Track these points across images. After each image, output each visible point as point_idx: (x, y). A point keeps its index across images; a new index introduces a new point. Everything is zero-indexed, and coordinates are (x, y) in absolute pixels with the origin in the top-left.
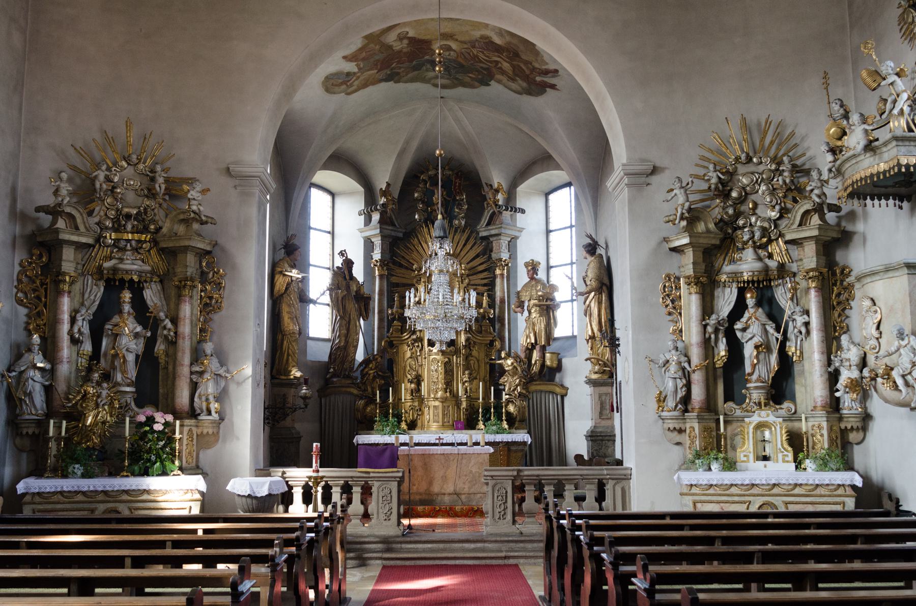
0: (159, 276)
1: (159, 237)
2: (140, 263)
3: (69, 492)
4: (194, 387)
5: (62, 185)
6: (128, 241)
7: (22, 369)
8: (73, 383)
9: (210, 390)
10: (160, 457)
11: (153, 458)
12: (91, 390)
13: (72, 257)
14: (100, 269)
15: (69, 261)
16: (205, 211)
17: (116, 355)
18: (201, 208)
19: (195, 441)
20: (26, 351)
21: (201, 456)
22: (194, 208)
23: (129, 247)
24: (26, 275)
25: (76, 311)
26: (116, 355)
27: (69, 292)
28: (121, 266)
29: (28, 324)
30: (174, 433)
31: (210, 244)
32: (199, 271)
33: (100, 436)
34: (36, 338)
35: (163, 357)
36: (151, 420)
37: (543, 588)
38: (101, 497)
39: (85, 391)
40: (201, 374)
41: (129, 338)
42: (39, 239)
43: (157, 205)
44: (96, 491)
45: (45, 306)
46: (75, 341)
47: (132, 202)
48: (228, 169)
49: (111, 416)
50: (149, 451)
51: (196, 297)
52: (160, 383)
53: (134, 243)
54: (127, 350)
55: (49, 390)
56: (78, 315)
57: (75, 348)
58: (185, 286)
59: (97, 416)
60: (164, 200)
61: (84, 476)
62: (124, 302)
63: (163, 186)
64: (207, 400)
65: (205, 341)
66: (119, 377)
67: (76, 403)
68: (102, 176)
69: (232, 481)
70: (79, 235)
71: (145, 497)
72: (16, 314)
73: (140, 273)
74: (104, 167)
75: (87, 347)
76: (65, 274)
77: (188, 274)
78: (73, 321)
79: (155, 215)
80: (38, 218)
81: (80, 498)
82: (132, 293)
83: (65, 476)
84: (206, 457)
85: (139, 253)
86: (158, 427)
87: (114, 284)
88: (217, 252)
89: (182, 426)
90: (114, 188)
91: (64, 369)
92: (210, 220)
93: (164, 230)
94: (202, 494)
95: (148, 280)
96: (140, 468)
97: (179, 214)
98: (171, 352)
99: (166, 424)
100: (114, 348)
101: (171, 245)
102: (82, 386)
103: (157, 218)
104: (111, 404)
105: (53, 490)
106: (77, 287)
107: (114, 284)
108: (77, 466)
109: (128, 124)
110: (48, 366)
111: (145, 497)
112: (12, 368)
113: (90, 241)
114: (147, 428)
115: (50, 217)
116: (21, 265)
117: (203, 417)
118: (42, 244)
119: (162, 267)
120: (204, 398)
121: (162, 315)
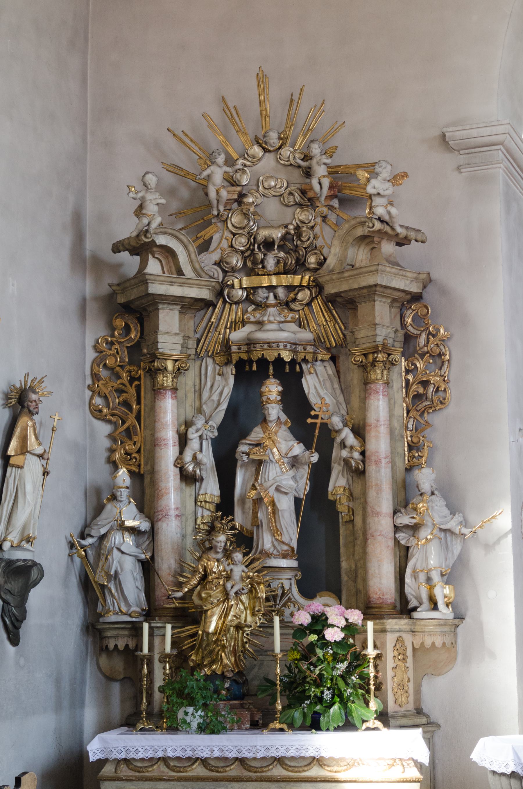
0: (328, 350)
1: (323, 276)
2: (293, 327)
3: (178, 759)
4: (403, 554)
5: (149, 197)
6: (271, 288)
7: (103, 531)
8: (189, 558)
9: (433, 562)
10: (340, 695)
11: (327, 695)
12: (215, 567)
13: (176, 328)
14: (226, 345)
15: (171, 332)
16: (403, 218)
17: (258, 501)
18: (394, 211)
19: (410, 660)
20: (109, 500)
21: (425, 688)
22: (380, 211)
23: (272, 300)
24: (105, 365)
25: (188, 424)
26: (258, 501)
27: (175, 390)
28: (261, 335)
29: (112, 451)
30: (365, 646)
31: (416, 279)
32: (401, 334)
33: (234, 652)
34: (123, 475)
35: (344, 500)
36: (319, 622)
37: (125, 301)
38: (234, 771)
39: (205, 569)
40: (415, 528)
41: (280, 471)
42: (121, 299)
43: (319, 220)
44: (226, 759)
45: (138, 418)
46: (188, 478)
47: (274, 218)
48: (444, 136)
49: (253, 615)
50: (319, 682)
51: (398, 383)
52: (342, 550)
53: (281, 292)
54: (278, 489)
55: (148, 568)
56: (191, 430)
57: (190, 491)
58: (373, 364)
59: (227, 615)
60: (331, 208)
61: (202, 729)
62: (268, 401)
63: (326, 183)
64: (429, 579)
65: (419, 466)
66: (267, 541)
67: (191, 591)
68: (218, 174)
69: (482, 741)
70: (183, 284)
71: (314, 772)
72: (93, 435)
73: (294, 346)
74: (221, 159)
75: (211, 488)
76: (165, 357)
77: (379, 339)
78: (183, 441)
79: (315, 237)
80: (120, 265)
81: (198, 770)
82: (282, 384)
83: (173, 729)
84: (435, 693)
85: (292, 310)
86: (333, 635)
87: (250, 370)
88: (431, 295)
89: (380, 632)
90: (242, 195)
91: (171, 530)
92: (412, 235)
93: (331, 262)
94: (420, 766)
95: (309, 357)
96: (305, 715)
97: (354, 227)
98: (357, 490)
99: (350, 629)
100: (254, 487)
101: (344, 287)
102: (199, 559)
103: (319, 242)
104: (252, 591)
105: (150, 755)
106: (189, 379)
107: (250, 370)
108: (190, 710)
109: (262, 80)
110: (145, 525)
111: (314, 772)
112: (86, 532)
113: (205, 294)
114: (313, 638)
115: (137, 258)
116: (96, 348)
117: (421, 614)
118: (127, 308)
119: (333, 332)
120: (422, 577)
121: (336, 421)
